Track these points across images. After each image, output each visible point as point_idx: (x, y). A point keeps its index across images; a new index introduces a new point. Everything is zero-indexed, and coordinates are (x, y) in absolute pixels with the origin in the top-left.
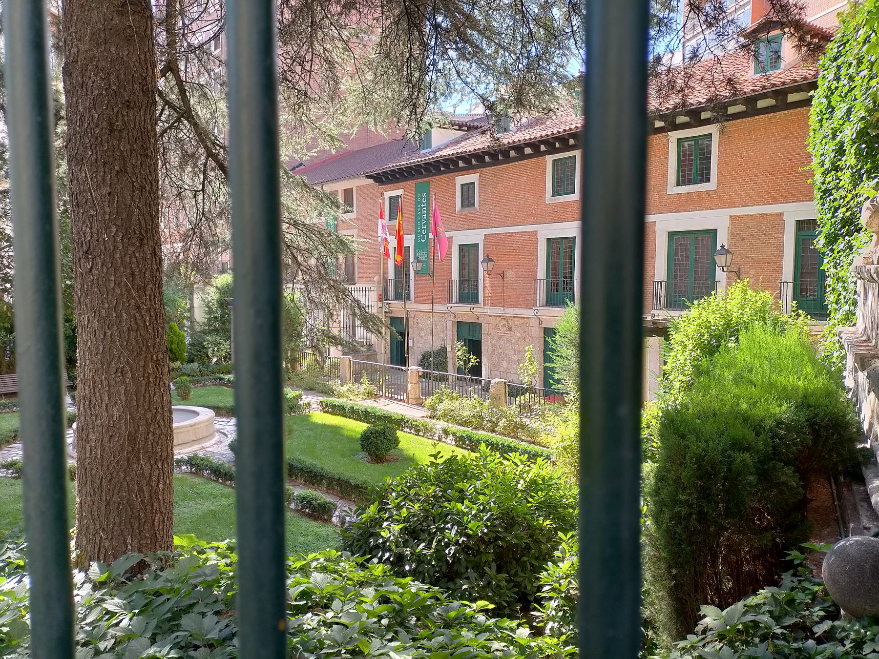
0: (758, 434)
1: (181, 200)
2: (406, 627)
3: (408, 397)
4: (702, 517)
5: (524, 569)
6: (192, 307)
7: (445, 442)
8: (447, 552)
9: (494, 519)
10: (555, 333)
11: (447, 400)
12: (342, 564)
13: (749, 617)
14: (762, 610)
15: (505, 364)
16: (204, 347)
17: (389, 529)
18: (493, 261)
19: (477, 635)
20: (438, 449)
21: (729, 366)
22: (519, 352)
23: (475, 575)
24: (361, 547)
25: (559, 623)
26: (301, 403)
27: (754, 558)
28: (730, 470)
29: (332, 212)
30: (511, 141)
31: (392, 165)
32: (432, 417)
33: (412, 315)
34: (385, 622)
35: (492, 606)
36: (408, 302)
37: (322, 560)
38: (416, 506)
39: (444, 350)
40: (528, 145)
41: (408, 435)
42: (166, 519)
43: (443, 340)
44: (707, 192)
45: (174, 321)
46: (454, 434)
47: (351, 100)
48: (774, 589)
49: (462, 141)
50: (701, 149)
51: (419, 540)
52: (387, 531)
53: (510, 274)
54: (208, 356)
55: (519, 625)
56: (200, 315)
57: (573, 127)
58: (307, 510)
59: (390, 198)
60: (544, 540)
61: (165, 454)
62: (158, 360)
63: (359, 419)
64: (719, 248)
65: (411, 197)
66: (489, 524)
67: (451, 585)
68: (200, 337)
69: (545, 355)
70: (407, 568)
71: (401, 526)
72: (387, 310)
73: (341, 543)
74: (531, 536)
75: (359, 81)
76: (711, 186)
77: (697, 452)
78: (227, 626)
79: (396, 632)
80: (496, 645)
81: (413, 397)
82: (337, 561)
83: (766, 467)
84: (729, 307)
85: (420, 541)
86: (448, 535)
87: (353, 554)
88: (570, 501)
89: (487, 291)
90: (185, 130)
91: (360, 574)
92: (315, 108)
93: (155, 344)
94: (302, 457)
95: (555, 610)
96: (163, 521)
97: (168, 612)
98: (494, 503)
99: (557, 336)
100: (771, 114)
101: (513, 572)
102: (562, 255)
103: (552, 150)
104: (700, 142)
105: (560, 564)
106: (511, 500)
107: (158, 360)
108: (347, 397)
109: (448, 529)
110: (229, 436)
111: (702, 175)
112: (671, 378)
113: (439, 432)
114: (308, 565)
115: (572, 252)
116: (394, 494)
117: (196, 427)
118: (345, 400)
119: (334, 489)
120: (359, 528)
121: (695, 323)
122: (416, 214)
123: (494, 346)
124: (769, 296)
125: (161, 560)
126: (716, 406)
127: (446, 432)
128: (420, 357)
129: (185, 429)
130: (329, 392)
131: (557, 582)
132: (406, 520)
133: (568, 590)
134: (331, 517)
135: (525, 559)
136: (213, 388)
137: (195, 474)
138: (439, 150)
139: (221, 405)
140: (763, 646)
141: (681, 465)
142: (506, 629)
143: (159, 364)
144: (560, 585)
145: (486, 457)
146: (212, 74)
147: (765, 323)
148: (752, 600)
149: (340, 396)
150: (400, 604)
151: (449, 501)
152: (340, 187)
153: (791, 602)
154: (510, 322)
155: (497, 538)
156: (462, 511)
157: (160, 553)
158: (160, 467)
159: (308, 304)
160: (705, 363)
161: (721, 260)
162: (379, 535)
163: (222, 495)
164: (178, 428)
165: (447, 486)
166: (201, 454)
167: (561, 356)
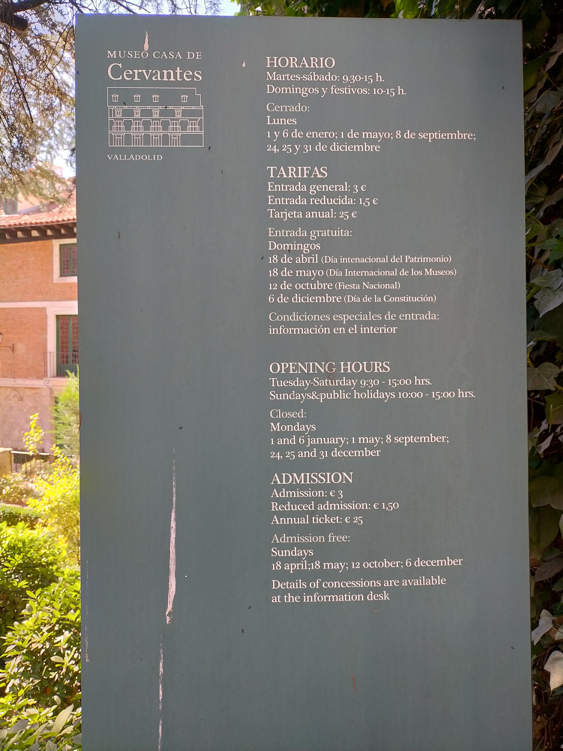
25: (20, 678)
53: (21, 348)
103: (58, 235)
154: (21, 393)
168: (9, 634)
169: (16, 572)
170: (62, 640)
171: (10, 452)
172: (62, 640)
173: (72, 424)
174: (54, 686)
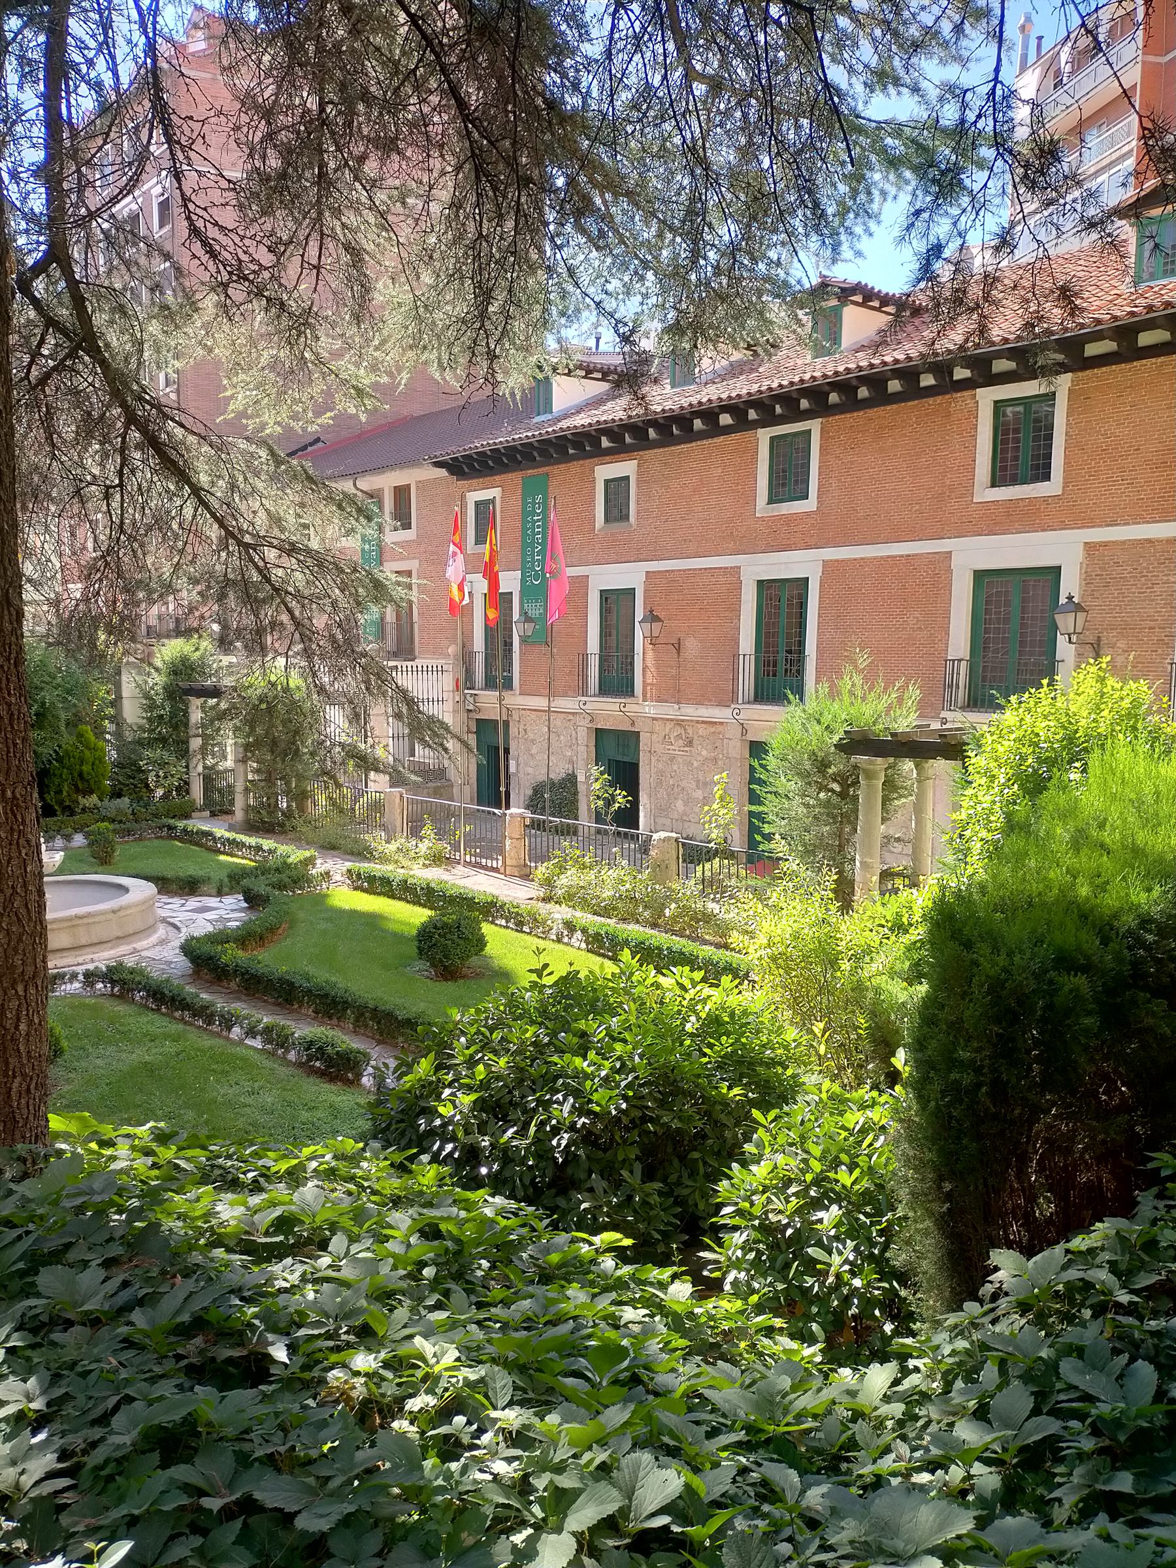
0: (1105, 941)
1: (82, 502)
2: (468, 1282)
3: (504, 862)
4: (999, 1090)
5: (693, 1174)
6: (119, 697)
7: (567, 944)
8: (554, 1143)
9: (641, 1086)
10: (766, 752)
11: (574, 870)
12: (365, 1164)
13: (1073, 1274)
14: (1098, 1260)
15: (680, 805)
16: (140, 770)
17: (453, 1102)
18: (659, 620)
19: (594, 1296)
20: (544, 958)
21: (1065, 815)
22: (705, 784)
23: (604, 1184)
24: (403, 1134)
25: (748, 1271)
26: (314, 872)
27: (1100, 1159)
28: (1049, 1007)
29: (360, 529)
30: (695, 402)
31: (481, 443)
32: (546, 899)
33: (516, 717)
34: (429, 1272)
35: (628, 1242)
36: (506, 694)
37: (328, 1157)
38: (502, 1062)
39: (571, 779)
40: (726, 408)
41: (503, 931)
42: (32, 1086)
43: (571, 762)
44: (1045, 499)
45: (86, 723)
46: (584, 931)
47: (394, 322)
48: (1121, 1223)
49: (608, 400)
50: (1037, 420)
51: (506, 1121)
52: (449, 1104)
53: (691, 646)
54: (147, 786)
55: (675, 1277)
56: (132, 712)
57: (807, 377)
58: (318, 1064)
59: (477, 504)
60: (730, 1122)
61: (30, 970)
62: (14, 797)
63: (416, 902)
64: (1063, 600)
65: (516, 502)
66: (631, 1093)
67: (562, 1202)
68: (134, 751)
69: (751, 791)
70: (484, 1171)
71: (473, 1097)
72: (471, 707)
73: (365, 1125)
74: (708, 1114)
75: (407, 287)
76: (1052, 487)
77: (992, 973)
78: (125, 1284)
79: (447, 1293)
80: (629, 1314)
81: (514, 863)
82: (354, 1159)
83: (1119, 1000)
84: (1073, 708)
85: (509, 1123)
86: (555, 1113)
87: (384, 1148)
88: (779, 1052)
89: (649, 674)
90: (87, 378)
91: (393, 1185)
92: (327, 335)
93: (9, 769)
94: (311, 970)
95: (742, 1248)
96: (28, 1091)
97: (20, 1259)
98: (641, 1056)
99: (770, 758)
100: (1161, 359)
101: (673, 1178)
102: (785, 609)
104: (1034, 407)
105: (753, 1168)
106: (672, 1051)
107: (14, 797)
108: (396, 862)
109: (557, 1102)
110: (184, 930)
111: (1037, 467)
112: (968, 833)
113: (557, 927)
114: (302, 1167)
115: (803, 605)
116: (463, 1039)
117: (121, 913)
118: (390, 867)
119: (366, 1026)
120: (402, 1099)
121: (1012, 737)
122: (524, 534)
123: (661, 773)
124: (1145, 689)
125: (24, 1161)
126: (1035, 887)
127: (570, 927)
128: (530, 792)
129: (102, 918)
130: (363, 853)
131: (748, 1199)
132: (484, 1085)
133: (766, 1213)
134: (359, 1076)
135: (696, 1155)
136: (156, 843)
137: (120, 997)
138: (566, 416)
139: (169, 874)
140: (1094, 1328)
141: (964, 995)
142: (651, 1284)
143: (18, 806)
144: (752, 1204)
145: (632, 974)
146: (134, 269)
147: (1136, 737)
148: (1079, 1243)
149: (384, 859)
150: (458, 1241)
151: (561, 1052)
152: (387, 482)
153: (1151, 1245)
154: (690, 731)
155: (645, 1119)
156: (583, 1071)
157: (21, 1148)
158: (21, 993)
159: (315, 696)
160: (1021, 809)
161: (1065, 622)
162: (434, 1113)
163: (166, 1036)
164: (55, 921)
165: (559, 1025)
166: (130, 962)
167: (776, 793)
168: (724, 1184)
169: (720, 1066)
170: (829, 1217)
171: (676, 840)
172: (829, 1217)
173: (791, 795)
174: (812, 1303)
